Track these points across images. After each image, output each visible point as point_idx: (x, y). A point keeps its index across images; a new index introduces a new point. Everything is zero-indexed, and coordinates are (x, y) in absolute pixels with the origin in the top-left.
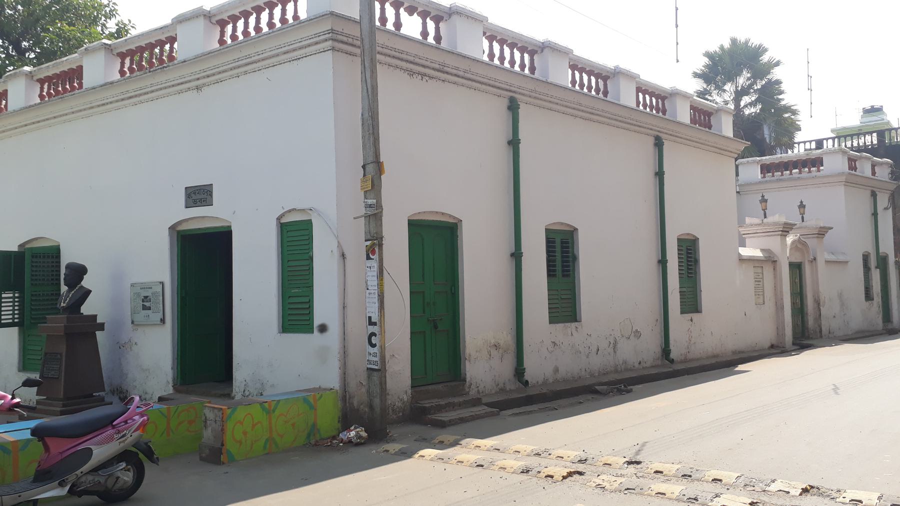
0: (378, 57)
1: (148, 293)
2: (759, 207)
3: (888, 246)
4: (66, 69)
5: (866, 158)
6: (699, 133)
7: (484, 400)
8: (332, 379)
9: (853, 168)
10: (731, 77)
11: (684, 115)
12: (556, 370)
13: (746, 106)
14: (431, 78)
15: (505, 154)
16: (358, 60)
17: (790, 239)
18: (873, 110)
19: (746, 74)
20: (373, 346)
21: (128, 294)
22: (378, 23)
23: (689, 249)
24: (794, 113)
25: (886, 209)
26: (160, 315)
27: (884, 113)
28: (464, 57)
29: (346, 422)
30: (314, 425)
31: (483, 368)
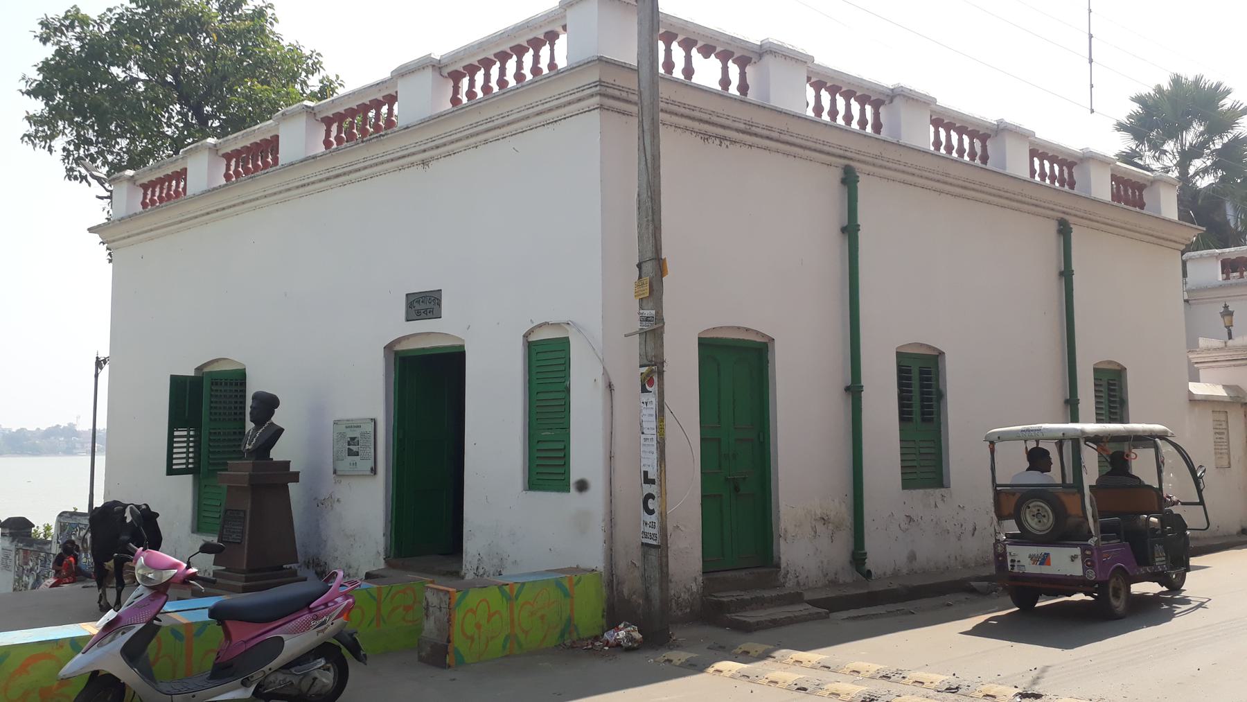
0: (662, 116)
1: (356, 434)
2: (1221, 323)
6: (1126, 215)
7: (807, 596)
8: (593, 556)
10: (1174, 132)
12: (912, 557)
13: (1196, 174)
14: (734, 142)
15: (836, 247)
20: (651, 512)
22: (661, 71)
26: (370, 464)
28: (780, 112)
29: (615, 613)
30: (570, 620)
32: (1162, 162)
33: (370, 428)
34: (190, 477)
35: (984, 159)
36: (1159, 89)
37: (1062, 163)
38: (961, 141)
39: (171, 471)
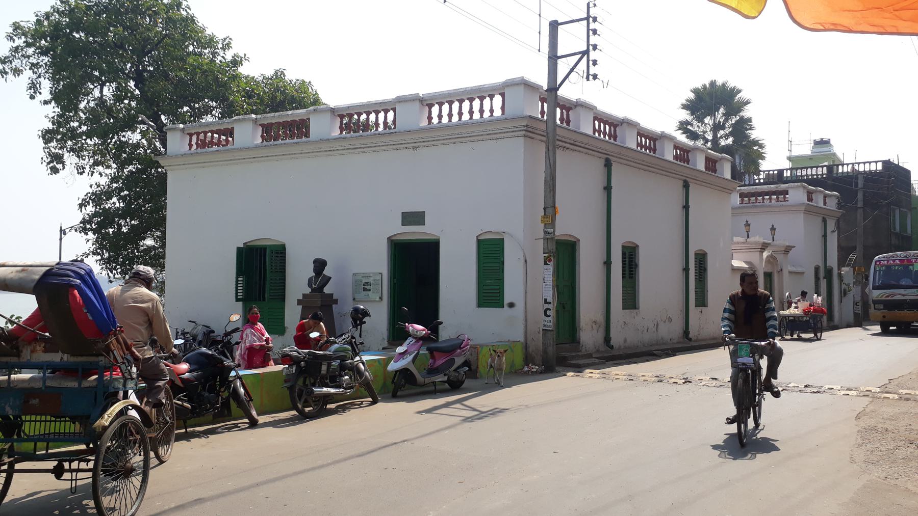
0: (558, 143)
2: (744, 229)
3: (833, 261)
5: (820, 191)
8: (518, 335)
9: (810, 199)
10: (712, 112)
11: (701, 165)
12: (625, 341)
13: (721, 137)
15: (601, 196)
16: (544, 145)
17: (765, 254)
18: (822, 143)
19: (722, 110)
22: (558, 122)
23: (701, 258)
24: (761, 146)
25: (833, 232)
27: (831, 145)
28: (582, 134)
29: (528, 359)
31: (589, 336)
33: (379, 277)
34: (241, 303)
35: (568, 122)
36: (705, 86)
37: (651, 139)
38: (605, 128)
39: (237, 300)
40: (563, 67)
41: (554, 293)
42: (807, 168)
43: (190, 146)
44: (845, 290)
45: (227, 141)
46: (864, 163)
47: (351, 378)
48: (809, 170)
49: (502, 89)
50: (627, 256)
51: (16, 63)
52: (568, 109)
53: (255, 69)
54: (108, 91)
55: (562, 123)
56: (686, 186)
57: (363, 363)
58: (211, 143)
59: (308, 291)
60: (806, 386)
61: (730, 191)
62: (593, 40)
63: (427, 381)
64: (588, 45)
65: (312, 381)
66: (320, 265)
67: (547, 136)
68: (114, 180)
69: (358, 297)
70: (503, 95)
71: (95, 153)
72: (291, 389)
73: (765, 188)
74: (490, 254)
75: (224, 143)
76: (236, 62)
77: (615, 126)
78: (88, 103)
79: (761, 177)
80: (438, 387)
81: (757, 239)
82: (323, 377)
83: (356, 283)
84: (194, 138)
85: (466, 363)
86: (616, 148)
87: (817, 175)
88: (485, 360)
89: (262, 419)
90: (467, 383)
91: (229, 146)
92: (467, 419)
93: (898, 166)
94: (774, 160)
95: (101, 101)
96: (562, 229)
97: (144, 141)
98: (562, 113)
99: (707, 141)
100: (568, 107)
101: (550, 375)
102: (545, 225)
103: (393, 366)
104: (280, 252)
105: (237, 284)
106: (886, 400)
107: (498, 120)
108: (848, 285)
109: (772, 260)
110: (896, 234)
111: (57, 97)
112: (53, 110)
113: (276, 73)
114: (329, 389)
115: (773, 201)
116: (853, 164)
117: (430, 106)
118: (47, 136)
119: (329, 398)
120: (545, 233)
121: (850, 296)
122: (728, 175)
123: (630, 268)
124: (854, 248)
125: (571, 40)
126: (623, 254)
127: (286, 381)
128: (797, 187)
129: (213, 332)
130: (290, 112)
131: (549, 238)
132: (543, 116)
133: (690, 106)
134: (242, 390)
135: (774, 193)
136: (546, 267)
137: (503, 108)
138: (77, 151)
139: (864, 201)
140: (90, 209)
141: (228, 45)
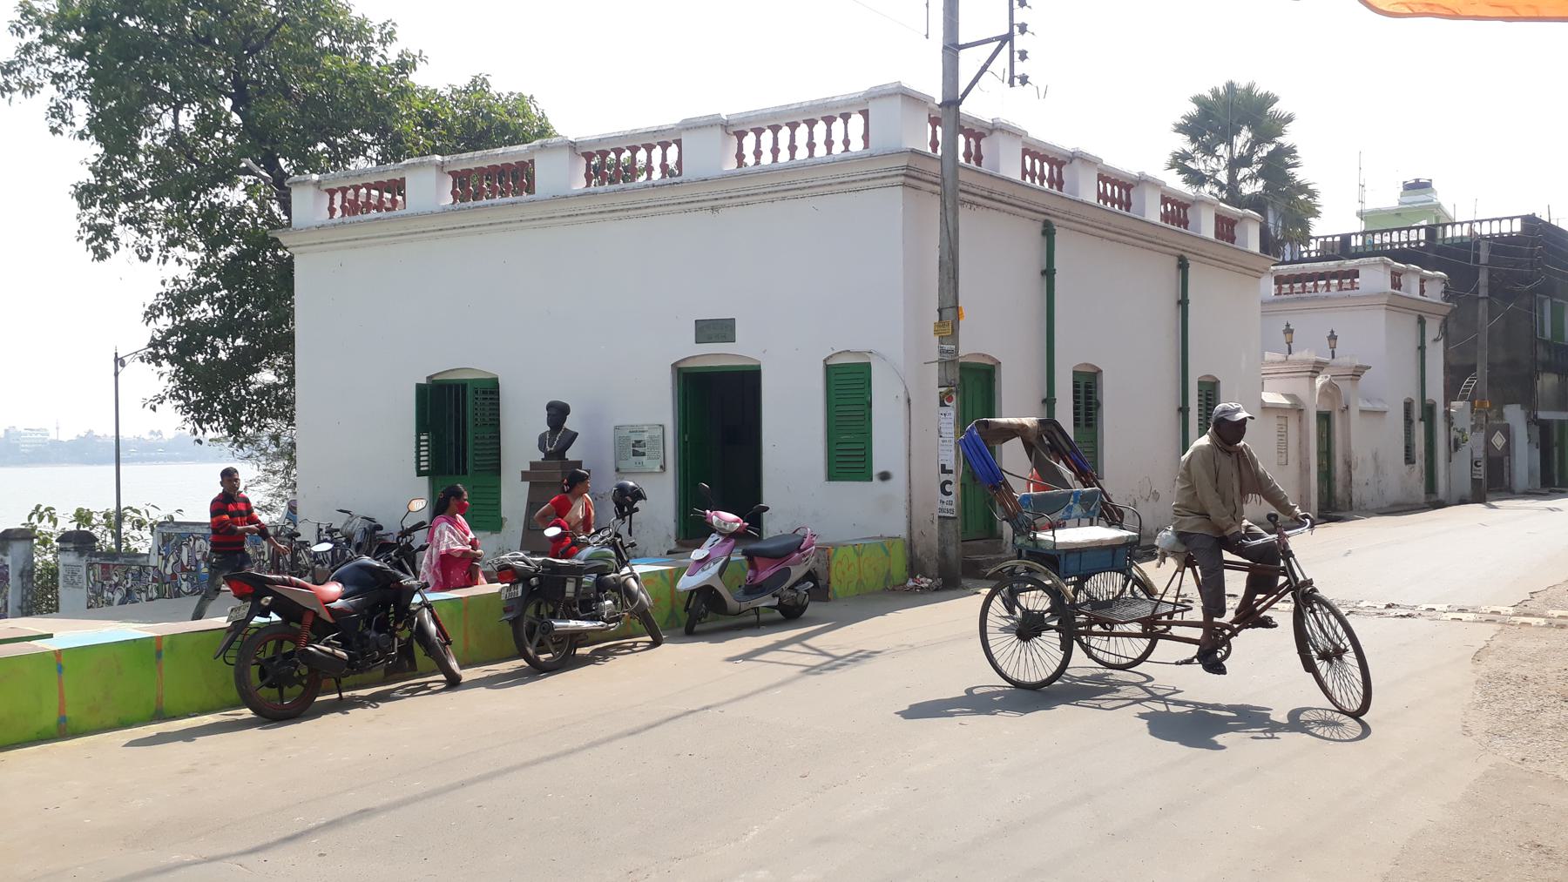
0: (962, 195)
2: (1282, 339)
3: (1436, 391)
4: (499, 163)
5: (1414, 271)
9: (1396, 285)
10: (1227, 137)
11: (1208, 230)
13: (1244, 180)
21: (609, 438)
22: (962, 159)
24: (1312, 194)
25: (1436, 340)
26: (659, 462)
27: (1433, 191)
28: (1002, 179)
29: (914, 567)
32: (1215, 165)
36: (1215, 92)
37: (1052, 162)
39: (420, 473)
40: (969, 62)
41: (957, 455)
42: (1391, 231)
43: (332, 211)
44: (1456, 440)
45: (394, 201)
46: (1491, 221)
47: (615, 603)
48: (1395, 234)
49: (864, 105)
50: (1082, 389)
51: (28, 72)
52: (979, 137)
53: (438, 76)
54: (187, 119)
55: (968, 160)
56: (1183, 265)
57: (636, 579)
58: (368, 206)
59: (539, 456)
60: (1389, 606)
61: (1258, 274)
62: (1020, 16)
63: (744, 606)
64: (1012, 25)
65: (551, 609)
66: (558, 413)
67: (943, 184)
68: (200, 272)
69: (623, 465)
70: (865, 114)
71: (167, 228)
72: (515, 623)
73: (1320, 266)
74: (848, 388)
75: (389, 205)
76: (405, 65)
77: (1060, 165)
78: (153, 138)
79: (1312, 247)
80: (762, 617)
81: (1305, 354)
82: (570, 603)
83: (620, 442)
84: (338, 198)
85: (810, 576)
86: (1063, 204)
87: (1409, 242)
88: (841, 575)
89: (467, 675)
90: (812, 609)
91: (398, 212)
92: (811, 670)
93: (1548, 225)
94: (1334, 220)
95: (176, 136)
96: (971, 346)
97: (251, 203)
98: (968, 144)
99: (1222, 187)
100: (978, 133)
101: (952, 593)
102: (941, 338)
103: (687, 582)
104: (490, 391)
105: (418, 446)
106: (1525, 628)
107: (859, 158)
108: (1462, 432)
109: (1331, 390)
110: (1545, 343)
111: (98, 128)
112: (93, 150)
113: (474, 81)
114: (580, 623)
115: (1333, 289)
116: (1471, 223)
117: (741, 135)
118: (85, 195)
119: (579, 638)
120: (942, 351)
121: (1465, 450)
122: (1254, 246)
123: (1088, 409)
124: (1473, 368)
125: (982, 14)
126: (1076, 385)
127: (506, 611)
128: (1375, 264)
129: (381, 528)
130: (500, 150)
131: (948, 360)
132: (935, 150)
133: (1191, 128)
134: (432, 627)
135: (1334, 275)
136: (944, 410)
137: (866, 137)
138: (138, 222)
139: (1490, 285)
140: (165, 322)
141: (390, 34)
